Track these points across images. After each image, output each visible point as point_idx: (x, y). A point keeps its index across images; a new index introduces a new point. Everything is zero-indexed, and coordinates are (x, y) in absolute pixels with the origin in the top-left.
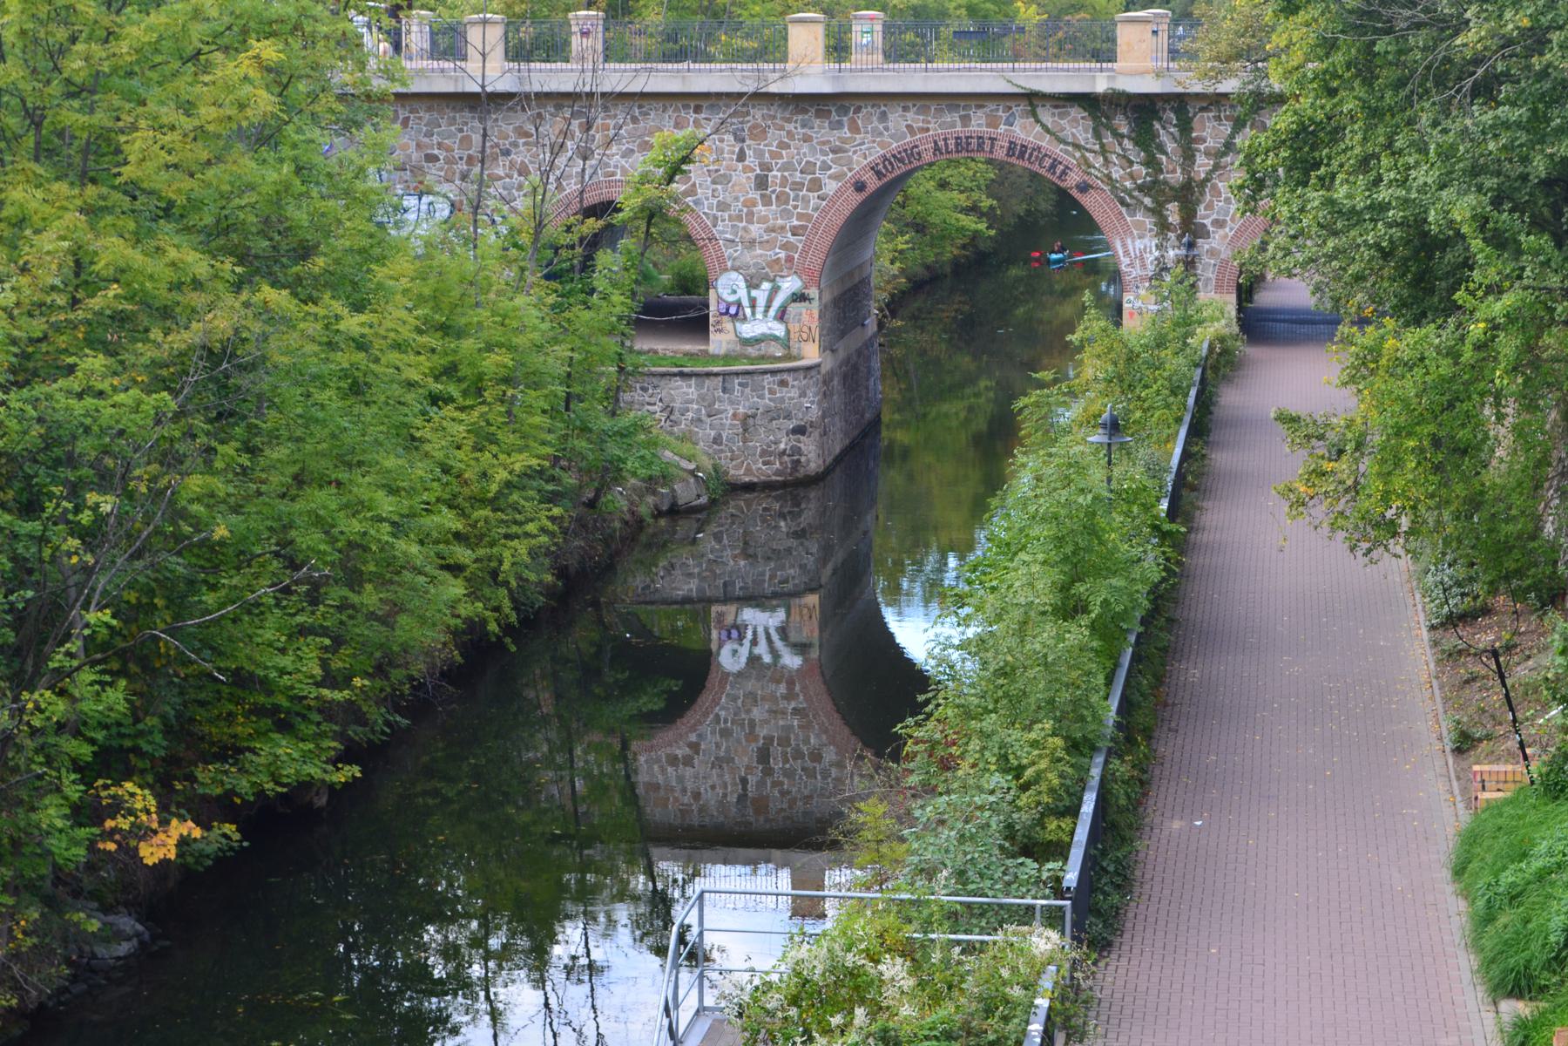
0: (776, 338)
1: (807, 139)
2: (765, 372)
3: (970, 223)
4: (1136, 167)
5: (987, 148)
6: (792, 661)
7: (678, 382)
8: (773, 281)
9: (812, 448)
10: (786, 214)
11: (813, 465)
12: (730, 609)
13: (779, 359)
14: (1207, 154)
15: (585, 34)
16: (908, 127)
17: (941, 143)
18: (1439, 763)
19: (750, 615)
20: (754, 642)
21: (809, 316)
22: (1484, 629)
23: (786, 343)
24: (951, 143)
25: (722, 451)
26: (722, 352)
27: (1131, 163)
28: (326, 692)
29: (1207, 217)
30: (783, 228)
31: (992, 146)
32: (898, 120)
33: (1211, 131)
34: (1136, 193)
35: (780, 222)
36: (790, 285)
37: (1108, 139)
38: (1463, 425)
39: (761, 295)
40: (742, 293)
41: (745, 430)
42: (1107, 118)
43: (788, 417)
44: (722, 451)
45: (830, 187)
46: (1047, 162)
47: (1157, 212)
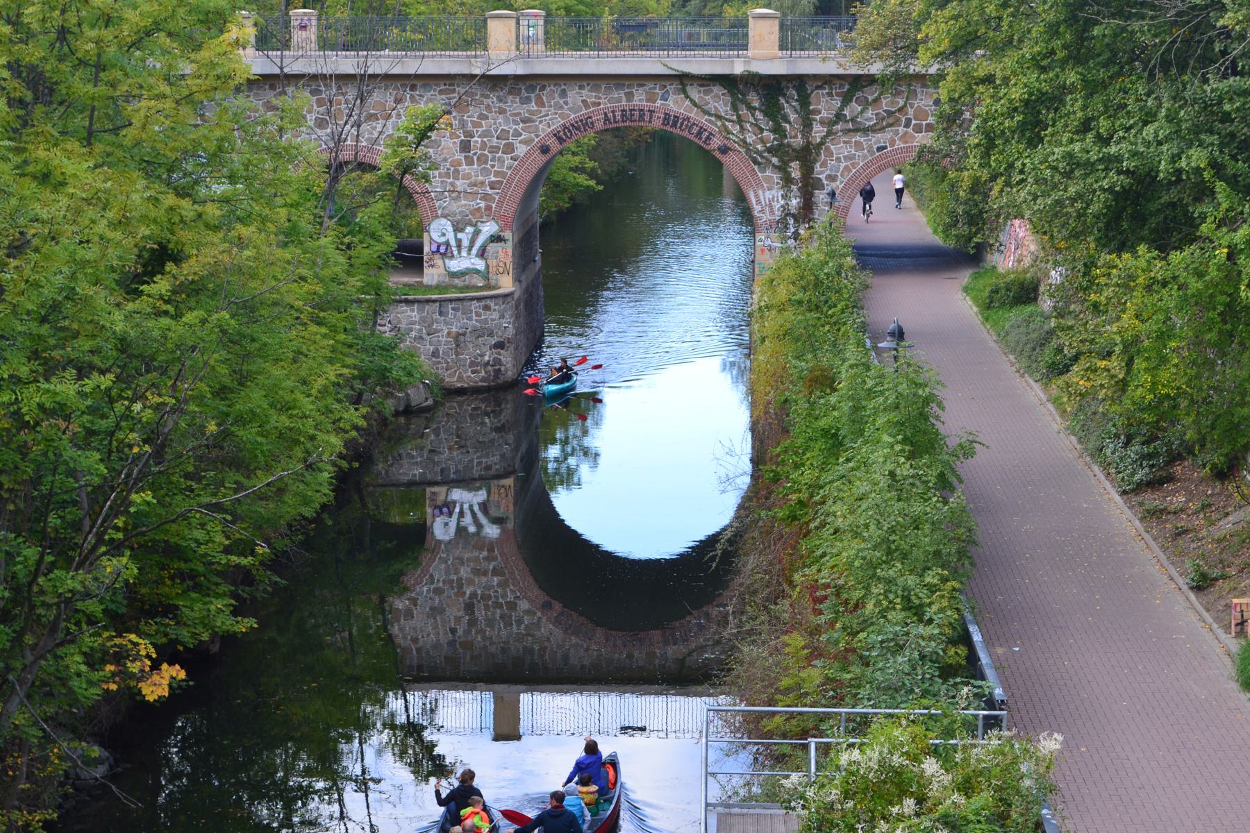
0: (477, 272)
1: (502, 111)
2: (472, 299)
3: (582, 180)
4: (765, 133)
5: (647, 119)
6: (492, 531)
7: (404, 307)
8: (475, 225)
9: (509, 359)
10: (486, 172)
11: (510, 373)
12: (441, 490)
13: (481, 289)
14: (822, 123)
15: (303, 28)
18: (1181, 599)
19: (457, 494)
20: (461, 514)
21: (505, 254)
22: (1175, 492)
23: (485, 275)
24: (618, 114)
25: (439, 363)
26: (434, 283)
27: (762, 130)
28: (234, 558)
29: (822, 173)
30: (483, 183)
31: (651, 117)
32: (576, 96)
33: (825, 105)
34: (766, 154)
35: (480, 178)
36: (489, 228)
37: (744, 111)
38: (1210, 330)
39: (465, 238)
40: (450, 236)
41: (457, 346)
42: (744, 95)
43: (491, 335)
44: (439, 363)
45: (521, 150)
46: (695, 130)
47: (783, 169)
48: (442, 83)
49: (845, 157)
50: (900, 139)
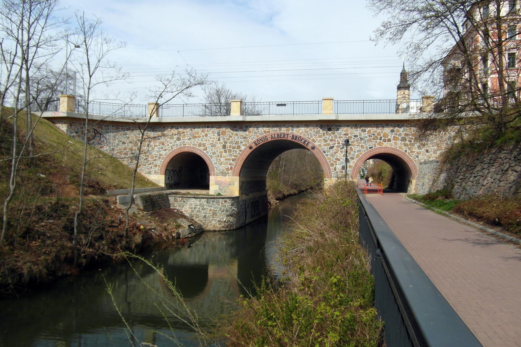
7: (194, 199)
10: (231, 155)
30: (230, 159)
32: (261, 130)
45: (243, 148)
46: (303, 141)
48: (217, 125)
49: (357, 151)
50: (378, 144)
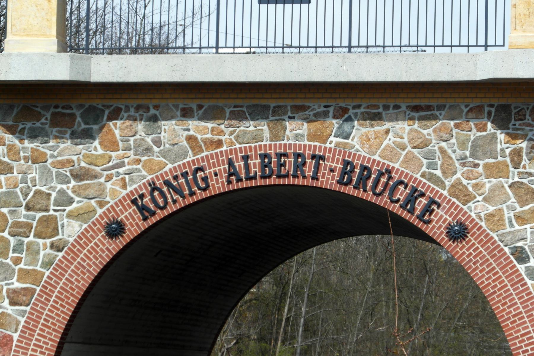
16: (189, 139)
17: (240, 164)
24: (255, 163)
31: (317, 167)
46: (402, 194)
